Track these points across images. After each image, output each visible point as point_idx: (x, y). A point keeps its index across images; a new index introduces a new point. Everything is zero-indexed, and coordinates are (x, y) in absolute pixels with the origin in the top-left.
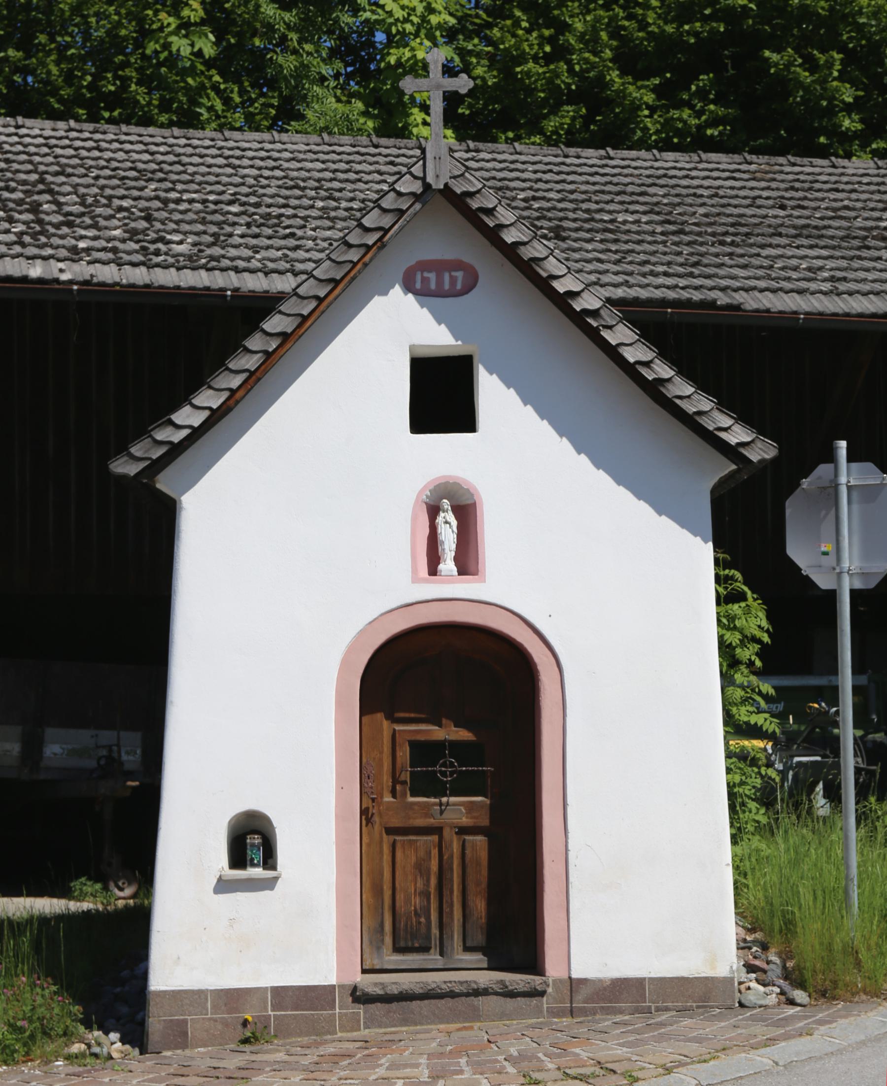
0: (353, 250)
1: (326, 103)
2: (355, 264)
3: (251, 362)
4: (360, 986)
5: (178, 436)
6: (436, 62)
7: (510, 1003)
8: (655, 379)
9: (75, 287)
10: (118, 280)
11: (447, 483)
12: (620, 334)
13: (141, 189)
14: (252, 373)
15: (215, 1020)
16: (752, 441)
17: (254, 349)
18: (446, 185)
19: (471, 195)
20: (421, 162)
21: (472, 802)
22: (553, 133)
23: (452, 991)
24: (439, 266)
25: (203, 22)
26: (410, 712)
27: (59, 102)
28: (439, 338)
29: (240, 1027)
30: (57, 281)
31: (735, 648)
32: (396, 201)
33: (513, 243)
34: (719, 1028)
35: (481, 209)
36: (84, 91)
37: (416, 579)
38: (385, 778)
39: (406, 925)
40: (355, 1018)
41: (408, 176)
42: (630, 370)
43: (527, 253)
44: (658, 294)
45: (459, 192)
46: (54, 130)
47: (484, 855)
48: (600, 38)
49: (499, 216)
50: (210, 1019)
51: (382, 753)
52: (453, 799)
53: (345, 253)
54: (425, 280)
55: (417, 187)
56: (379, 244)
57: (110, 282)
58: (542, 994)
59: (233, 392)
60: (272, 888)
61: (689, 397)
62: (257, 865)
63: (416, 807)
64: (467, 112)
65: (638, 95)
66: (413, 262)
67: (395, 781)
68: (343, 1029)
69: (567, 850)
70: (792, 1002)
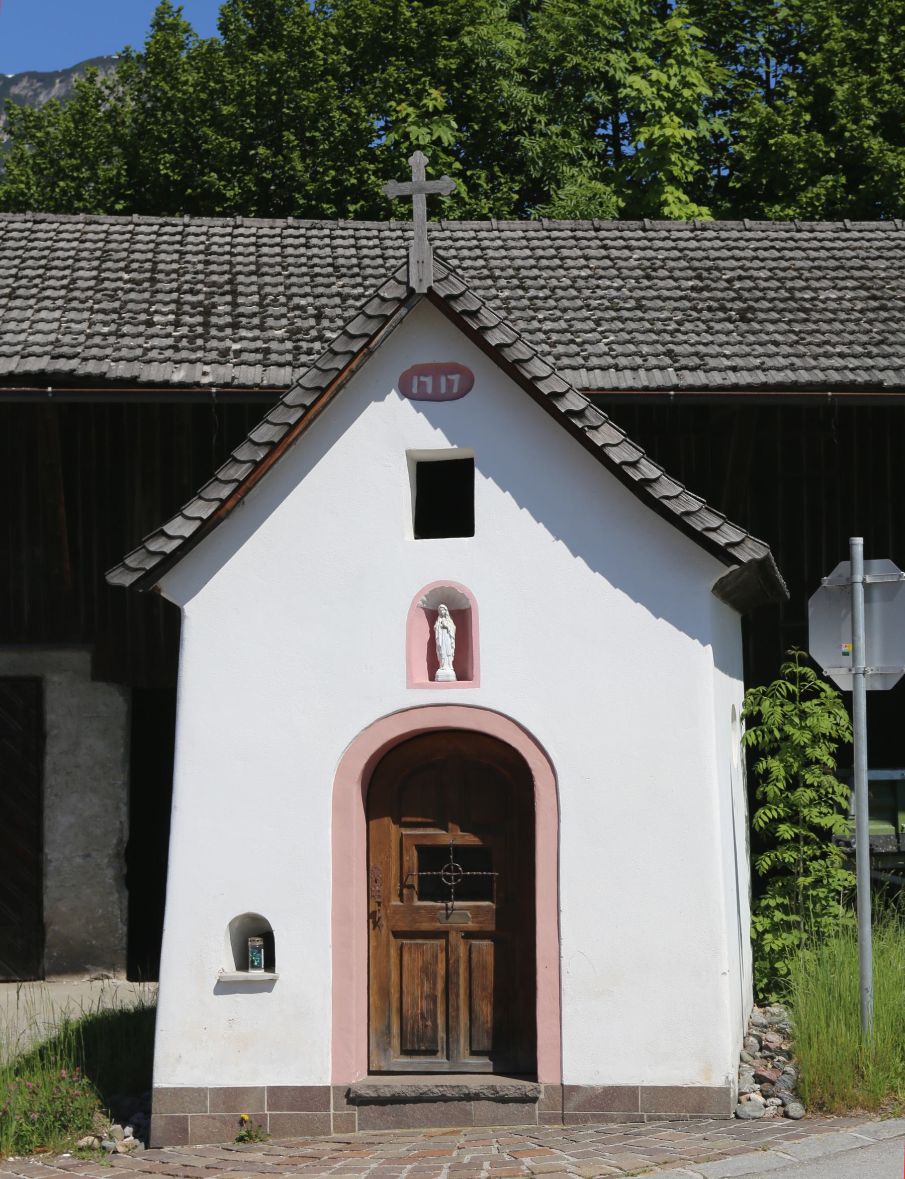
0: (339, 357)
1: (577, 185)
2: (341, 372)
3: (239, 472)
4: (353, 1089)
5: (170, 547)
6: (418, 165)
7: (502, 1108)
8: (641, 480)
9: (214, 390)
10: (258, 381)
11: (442, 588)
12: (607, 435)
13: (328, 286)
14: (241, 483)
15: (214, 1118)
16: (742, 541)
17: (242, 459)
18: (430, 289)
19: (455, 298)
20: (405, 267)
21: (478, 907)
22: (808, 204)
23: (443, 1095)
24: (436, 370)
25: (447, 110)
26: (417, 816)
27: (304, 197)
28: (436, 443)
29: (237, 1125)
30: (198, 384)
31: (804, 747)
32: (380, 306)
33: (497, 345)
34: (721, 1138)
35: (465, 312)
36: (329, 186)
37: (411, 684)
38: (393, 882)
39: (413, 1028)
40: (350, 1119)
41: (392, 281)
42: (617, 470)
43: (511, 355)
44: (819, 376)
45: (442, 295)
46: (272, 228)
47: (490, 960)
48: (863, 105)
49: (483, 318)
50: (209, 1117)
51: (389, 856)
52: (458, 904)
53: (331, 360)
54: (422, 385)
55: (400, 292)
56: (365, 350)
57: (250, 383)
58: (534, 1100)
59: (223, 502)
60: (270, 991)
61: (676, 497)
62: (258, 967)
63: (423, 911)
64: (738, 185)
65: (895, 162)
66: (409, 367)
67: (403, 885)
68: (337, 1129)
69: (560, 957)
70: (786, 1115)
